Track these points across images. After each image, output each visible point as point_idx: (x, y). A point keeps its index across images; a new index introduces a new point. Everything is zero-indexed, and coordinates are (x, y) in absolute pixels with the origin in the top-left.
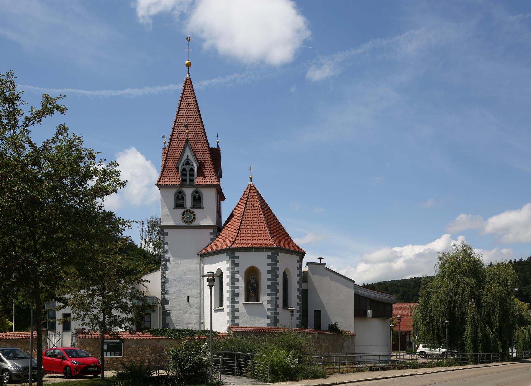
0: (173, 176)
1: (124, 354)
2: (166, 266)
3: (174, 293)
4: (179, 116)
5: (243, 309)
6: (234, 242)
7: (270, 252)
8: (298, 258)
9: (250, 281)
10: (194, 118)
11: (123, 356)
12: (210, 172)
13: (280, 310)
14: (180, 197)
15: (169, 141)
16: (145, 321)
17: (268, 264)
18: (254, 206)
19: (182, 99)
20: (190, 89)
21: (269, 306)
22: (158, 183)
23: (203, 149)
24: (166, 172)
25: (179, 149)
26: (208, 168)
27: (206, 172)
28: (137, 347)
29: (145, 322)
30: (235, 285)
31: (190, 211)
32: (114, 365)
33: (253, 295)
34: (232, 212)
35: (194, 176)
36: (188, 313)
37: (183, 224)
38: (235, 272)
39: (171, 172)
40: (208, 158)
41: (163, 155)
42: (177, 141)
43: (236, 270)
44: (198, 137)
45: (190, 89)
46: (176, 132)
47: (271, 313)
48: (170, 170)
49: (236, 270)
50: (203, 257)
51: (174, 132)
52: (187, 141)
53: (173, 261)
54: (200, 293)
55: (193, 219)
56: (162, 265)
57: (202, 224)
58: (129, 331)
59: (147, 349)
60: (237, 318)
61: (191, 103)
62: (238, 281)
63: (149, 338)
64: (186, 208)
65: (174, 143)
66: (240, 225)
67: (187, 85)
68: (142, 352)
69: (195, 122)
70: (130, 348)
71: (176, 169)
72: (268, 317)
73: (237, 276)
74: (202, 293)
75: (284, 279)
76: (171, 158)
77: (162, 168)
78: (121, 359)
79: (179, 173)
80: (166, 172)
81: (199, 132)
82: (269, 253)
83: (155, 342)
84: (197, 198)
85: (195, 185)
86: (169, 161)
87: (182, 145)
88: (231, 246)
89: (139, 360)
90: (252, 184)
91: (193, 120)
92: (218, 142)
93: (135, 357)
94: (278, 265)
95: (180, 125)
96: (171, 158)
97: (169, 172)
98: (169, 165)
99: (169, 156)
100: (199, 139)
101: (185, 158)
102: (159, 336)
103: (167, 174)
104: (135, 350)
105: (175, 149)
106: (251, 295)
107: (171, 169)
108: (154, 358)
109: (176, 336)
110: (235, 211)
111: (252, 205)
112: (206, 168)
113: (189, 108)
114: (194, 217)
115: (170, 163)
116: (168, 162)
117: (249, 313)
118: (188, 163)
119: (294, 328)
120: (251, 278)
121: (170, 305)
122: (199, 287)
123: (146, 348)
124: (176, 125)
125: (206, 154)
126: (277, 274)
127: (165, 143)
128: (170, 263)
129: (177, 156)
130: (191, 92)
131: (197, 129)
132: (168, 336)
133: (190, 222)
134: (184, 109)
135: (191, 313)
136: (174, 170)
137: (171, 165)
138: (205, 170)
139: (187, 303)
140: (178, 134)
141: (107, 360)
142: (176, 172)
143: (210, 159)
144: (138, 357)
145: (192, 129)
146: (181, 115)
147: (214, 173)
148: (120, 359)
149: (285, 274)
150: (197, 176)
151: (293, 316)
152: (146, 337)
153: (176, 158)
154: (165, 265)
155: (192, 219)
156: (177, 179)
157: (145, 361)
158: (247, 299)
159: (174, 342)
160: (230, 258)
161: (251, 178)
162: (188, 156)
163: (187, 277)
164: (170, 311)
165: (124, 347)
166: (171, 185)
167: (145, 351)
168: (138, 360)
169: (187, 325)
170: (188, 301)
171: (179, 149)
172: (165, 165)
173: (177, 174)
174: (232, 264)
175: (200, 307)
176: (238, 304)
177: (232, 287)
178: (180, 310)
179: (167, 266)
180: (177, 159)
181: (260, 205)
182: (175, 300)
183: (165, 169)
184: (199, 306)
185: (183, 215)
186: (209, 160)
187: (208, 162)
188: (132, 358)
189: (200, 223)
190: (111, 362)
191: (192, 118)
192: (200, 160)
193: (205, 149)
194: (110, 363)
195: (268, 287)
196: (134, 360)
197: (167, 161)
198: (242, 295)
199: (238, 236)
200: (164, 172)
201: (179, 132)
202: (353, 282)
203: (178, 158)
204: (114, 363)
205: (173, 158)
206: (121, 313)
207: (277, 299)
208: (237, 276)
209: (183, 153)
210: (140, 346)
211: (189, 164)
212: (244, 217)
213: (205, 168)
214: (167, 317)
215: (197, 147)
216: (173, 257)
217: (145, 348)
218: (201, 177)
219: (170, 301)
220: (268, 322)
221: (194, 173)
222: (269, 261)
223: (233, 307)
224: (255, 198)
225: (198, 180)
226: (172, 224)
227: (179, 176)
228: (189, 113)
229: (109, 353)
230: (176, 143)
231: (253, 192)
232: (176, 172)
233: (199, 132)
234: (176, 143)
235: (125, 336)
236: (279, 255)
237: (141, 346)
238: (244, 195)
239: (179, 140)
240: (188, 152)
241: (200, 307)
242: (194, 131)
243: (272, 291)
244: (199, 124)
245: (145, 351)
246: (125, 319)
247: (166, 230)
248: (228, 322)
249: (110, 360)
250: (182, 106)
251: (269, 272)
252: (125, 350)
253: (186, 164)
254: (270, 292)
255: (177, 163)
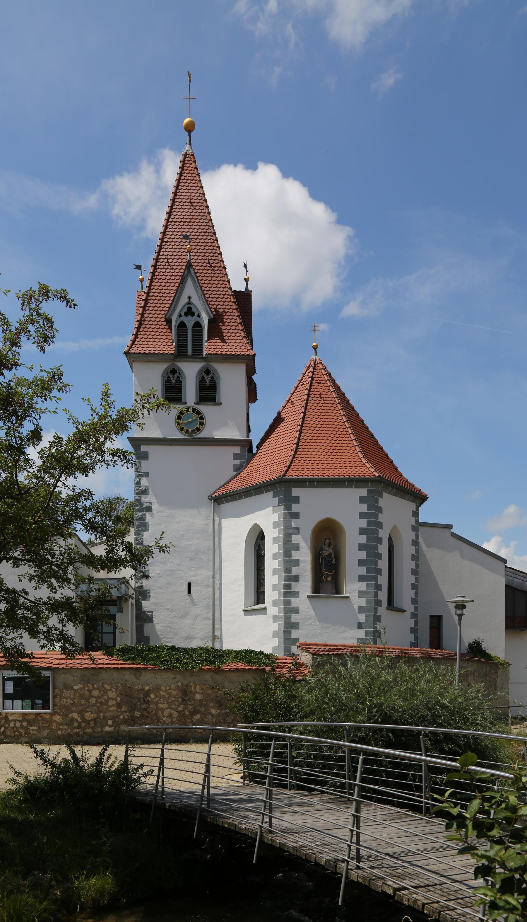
0: (160, 337)
1: (54, 705)
2: (145, 520)
3: (159, 575)
4: (172, 222)
5: (307, 609)
6: (289, 467)
7: (366, 489)
8: (412, 506)
9: (322, 549)
10: (202, 227)
11: (53, 709)
12: (236, 331)
13: (382, 610)
14: (173, 381)
15: (149, 276)
16: (102, 630)
17: (362, 515)
18: (325, 399)
19: (178, 191)
20: (192, 172)
21: (363, 602)
22: (129, 350)
23: (219, 286)
24: (146, 330)
25: (172, 284)
26: (231, 324)
27: (226, 331)
28: (87, 689)
29: (102, 633)
30: (293, 558)
31: (194, 410)
32: (31, 731)
33: (329, 579)
34: (279, 413)
35: (202, 337)
36: (188, 617)
37: (179, 435)
38: (291, 531)
39: (155, 330)
40: (230, 304)
41: (138, 302)
42: (168, 270)
43: (293, 525)
44: (209, 263)
45: (192, 172)
46: (166, 253)
47: (366, 616)
48: (153, 326)
49: (293, 525)
50: (219, 504)
51: (161, 253)
52: (189, 265)
53: (159, 512)
54: (214, 577)
55: (200, 427)
56: (137, 520)
57: (218, 435)
58: (60, 644)
59: (109, 693)
60: (296, 626)
61: (195, 198)
62: (299, 550)
63: (116, 668)
64: (186, 403)
65: (161, 274)
66: (300, 435)
67: (186, 165)
68: (100, 700)
69: (202, 234)
70: (69, 692)
71: (165, 323)
72: (360, 626)
73: (295, 539)
74: (218, 577)
75: (262, 597)
76: (156, 301)
77: (137, 321)
78: (47, 717)
79: (171, 332)
80: (146, 330)
81: (212, 255)
82: (363, 492)
83: (129, 677)
84: (208, 382)
85: (204, 355)
86: (151, 308)
87: (177, 278)
88: (284, 475)
89: (92, 720)
90: (317, 358)
91: (200, 231)
92: (247, 280)
93: (81, 713)
94: (381, 518)
95: (174, 240)
96: (156, 301)
97: (150, 330)
98: (151, 316)
99: (156, 278)
100: (211, 266)
101: (184, 300)
102: (139, 664)
103: (148, 333)
104: (82, 696)
105: (163, 284)
106: (325, 580)
107: (155, 323)
108: (127, 715)
109: (180, 663)
110: (284, 411)
111: (321, 398)
112: (226, 324)
113: (192, 207)
114: (201, 421)
115: (153, 312)
116: (148, 310)
117: (321, 618)
118: (190, 312)
119: (406, 648)
120: (325, 545)
121: (152, 600)
122: (212, 564)
123: (108, 690)
124: (165, 240)
125: (226, 296)
126: (379, 536)
127: (142, 280)
128: (152, 516)
129: (167, 298)
130: (194, 178)
131: (207, 248)
132: (162, 662)
133: (193, 432)
134: (182, 210)
135: (196, 617)
136: (162, 327)
137: (156, 316)
138: (223, 328)
139: (187, 597)
140: (169, 257)
141: (15, 718)
142: (165, 330)
143: (234, 307)
144: (88, 712)
145: (198, 247)
146: (175, 220)
147: (242, 332)
148: (45, 716)
149: (390, 539)
150: (209, 339)
151: (463, 617)
152: (108, 664)
153: (165, 302)
154: (142, 519)
155: (198, 425)
156: (168, 344)
157: (107, 722)
158: (317, 588)
159: (175, 678)
160: (280, 502)
161: (315, 348)
162: (189, 298)
163: (187, 543)
164: (152, 612)
165: (54, 689)
166: (156, 354)
167: (105, 697)
168: (90, 721)
169: (187, 641)
170: (189, 592)
171: (172, 284)
172: (142, 315)
173: (167, 334)
174: (284, 513)
175: (214, 604)
176: (298, 597)
177: (286, 562)
178: (172, 610)
179: (147, 521)
180: (168, 305)
181: (336, 397)
182: (162, 591)
183: (142, 324)
184: (211, 603)
185: (179, 418)
186: (232, 307)
187: (231, 311)
188: (75, 715)
189: (215, 433)
190: (25, 724)
191: (198, 227)
192: (213, 307)
193: (223, 286)
194: (22, 727)
195: (361, 563)
196: (79, 720)
197: (147, 308)
198: (306, 579)
199: (297, 456)
200: (141, 329)
201: (170, 253)
202: (504, 561)
203: (170, 302)
204: (31, 726)
205: (160, 302)
206: (33, 583)
207: (378, 587)
208: (295, 539)
209: (179, 289)
210: (93, 685)
211: (193, 314)
212: (305, 419)
213: (224, 323)
214: (146, 625)
215: (207, 282)
216: (160, 503)
217: (106, 691)
218: (217, 341)
219: (152, 592)
220: (359, 636)
221: (202, 332)
222: (364, 508)
223: (287, 603)
224: (326, 385)
225: (211, 347)
226: (157, 434)
227: (171, 338)
228: (191, 217)
229: (18, 703)
230: (166, 274)
231: (320, 374)
232: (165, 330)
233: (212, 255)
234: (166, 274)
235: (57, 662)
236: (382, 498)
237: (95, 686)
238: (302, 380)
239: (172, 269)
240: (190, 289)
241: (214, 604)
242: (202, 252)
243: (368, 570)
244: (211, 239)
245: (105, 697)
246: (45, 604)
247: (144, 448)
248: (275, 634)
249: (21, 719)
250: (177, 204)
251: (362, 531)
252: (56, 695)
253: (186, 314)
254: (364, 573)
255: (175, 296)
